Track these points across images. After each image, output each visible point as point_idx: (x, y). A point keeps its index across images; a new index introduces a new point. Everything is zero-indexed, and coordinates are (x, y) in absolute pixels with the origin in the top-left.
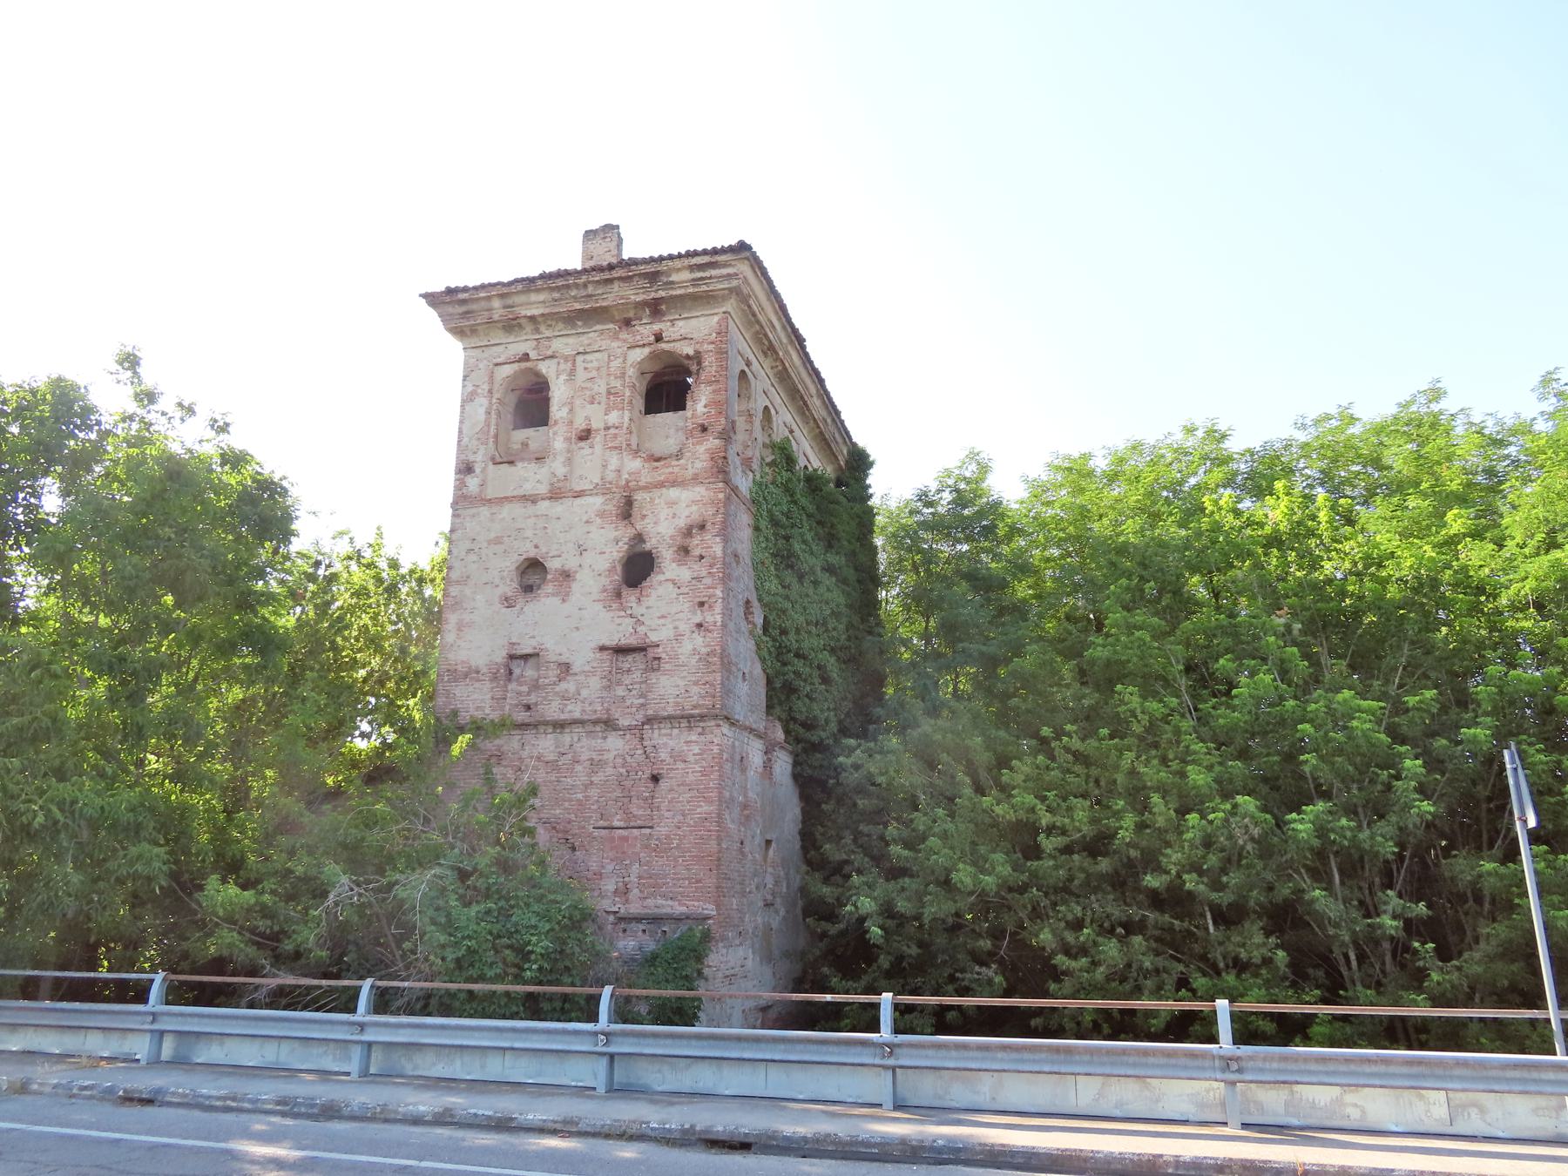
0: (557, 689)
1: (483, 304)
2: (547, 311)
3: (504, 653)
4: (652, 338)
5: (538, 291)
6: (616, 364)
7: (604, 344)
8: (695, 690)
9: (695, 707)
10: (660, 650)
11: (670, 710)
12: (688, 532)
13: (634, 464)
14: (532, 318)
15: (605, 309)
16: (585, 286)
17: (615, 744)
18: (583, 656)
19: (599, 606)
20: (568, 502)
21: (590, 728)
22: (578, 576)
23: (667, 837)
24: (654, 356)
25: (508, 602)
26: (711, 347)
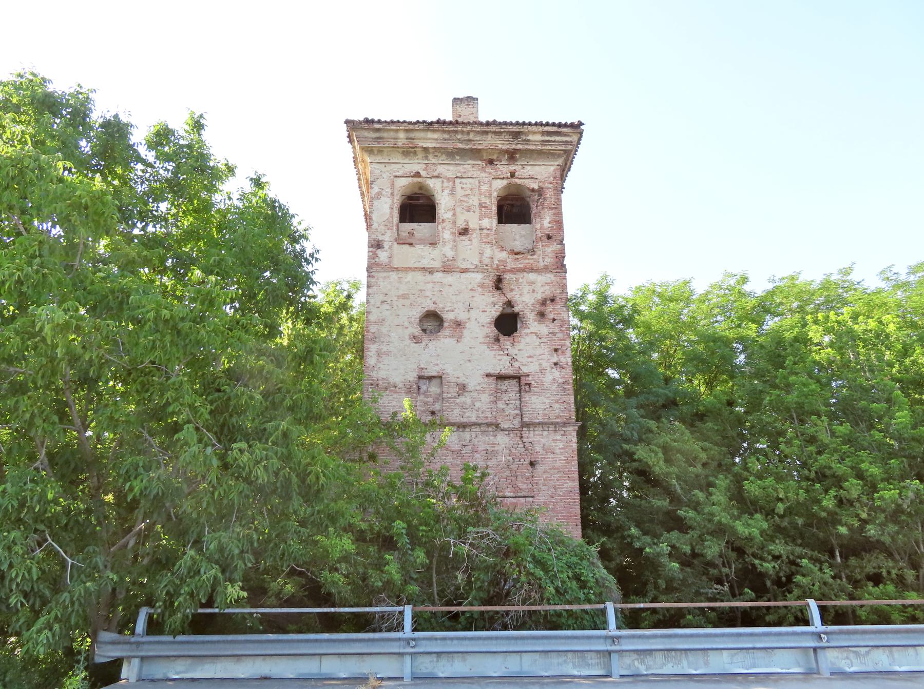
0: (458, 401)
1: (392, 134)
2: (438, 146)
3: (415, 375)
4: (509, 175)
5: (434, 131)
6: (485, 188)
7: (476, 173)
8: (556, 406)
9: (557, 417)
10: (530, 378)
11: (540, 419)
12: (544, 303)
13: (504, 255)
14: (426, 149)
15: (479, 151)
16: (468, 133)
17: (503, 441)
18: (475, 380)
19: (485, 347)
20: (456, 275)
21: (484, 428)
22: (467, 325)
23: (545, 503)
24: (508, 186)
25: (416, 339)
26: (550, 186)
